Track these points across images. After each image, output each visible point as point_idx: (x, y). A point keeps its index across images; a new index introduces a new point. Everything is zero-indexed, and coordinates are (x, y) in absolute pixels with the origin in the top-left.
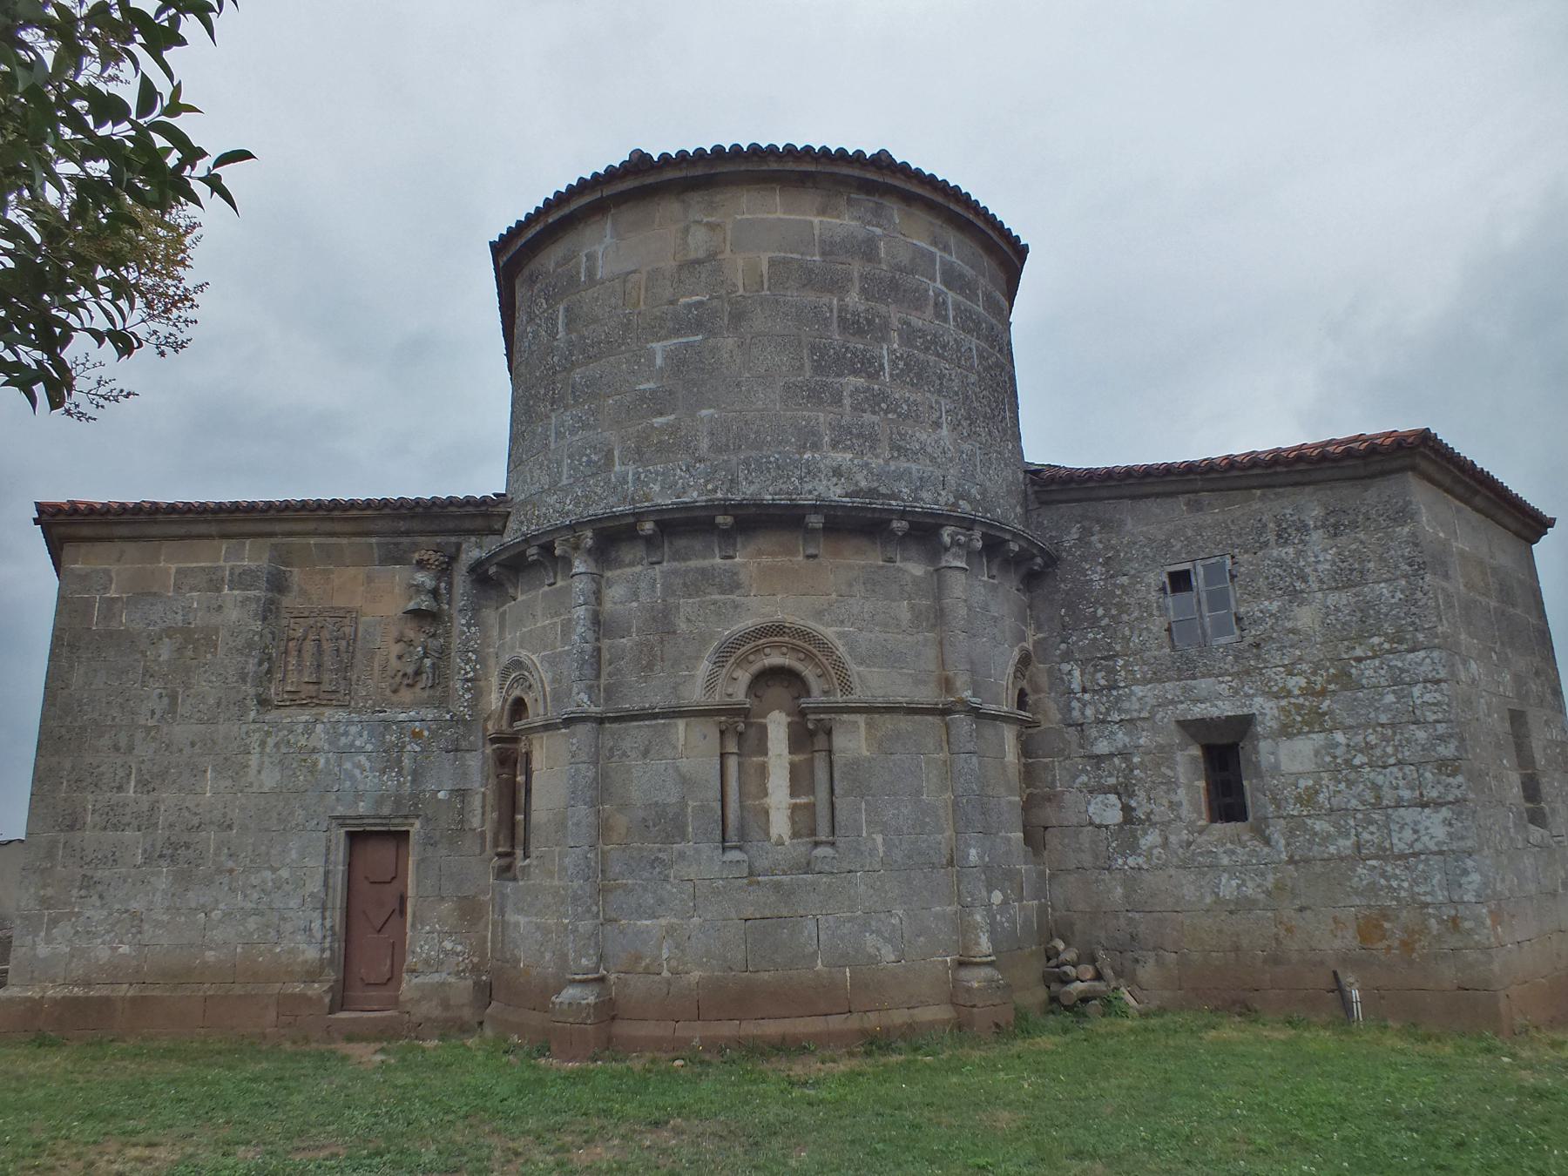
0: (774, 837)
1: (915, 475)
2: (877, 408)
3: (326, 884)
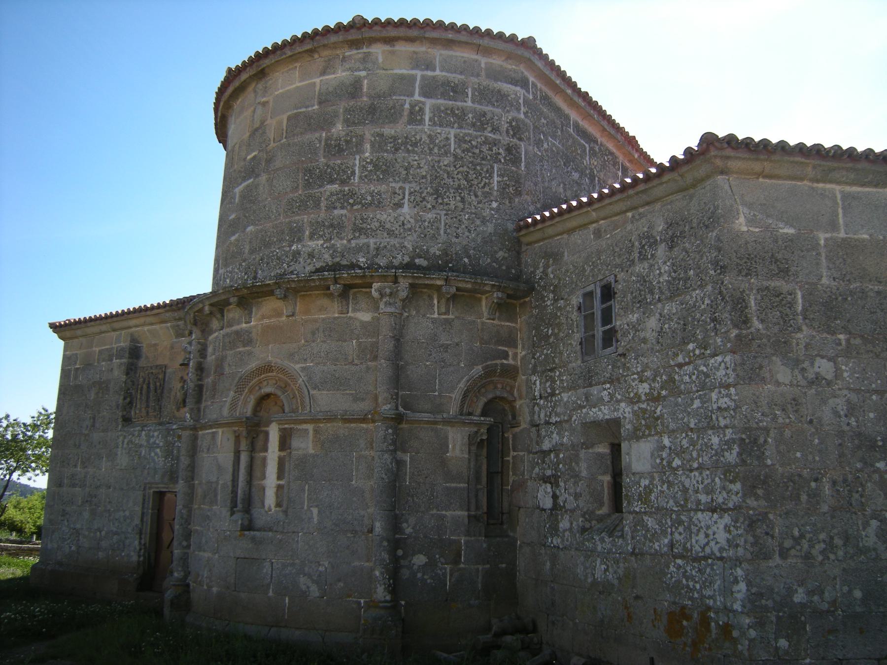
0: (266, 508)
1: (372, 246)
2: (346, 204)
3: (142, 520)
